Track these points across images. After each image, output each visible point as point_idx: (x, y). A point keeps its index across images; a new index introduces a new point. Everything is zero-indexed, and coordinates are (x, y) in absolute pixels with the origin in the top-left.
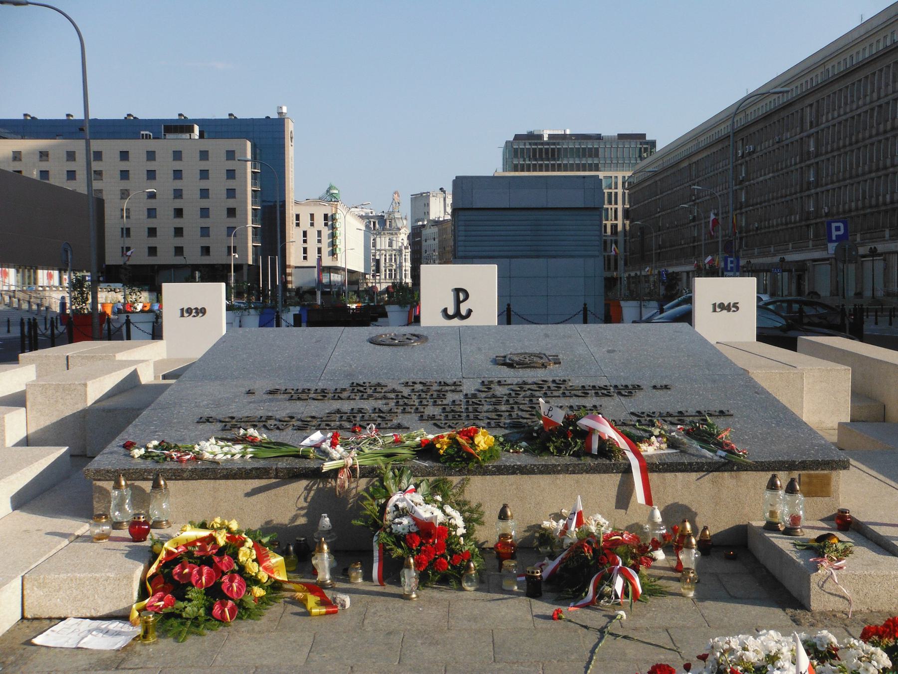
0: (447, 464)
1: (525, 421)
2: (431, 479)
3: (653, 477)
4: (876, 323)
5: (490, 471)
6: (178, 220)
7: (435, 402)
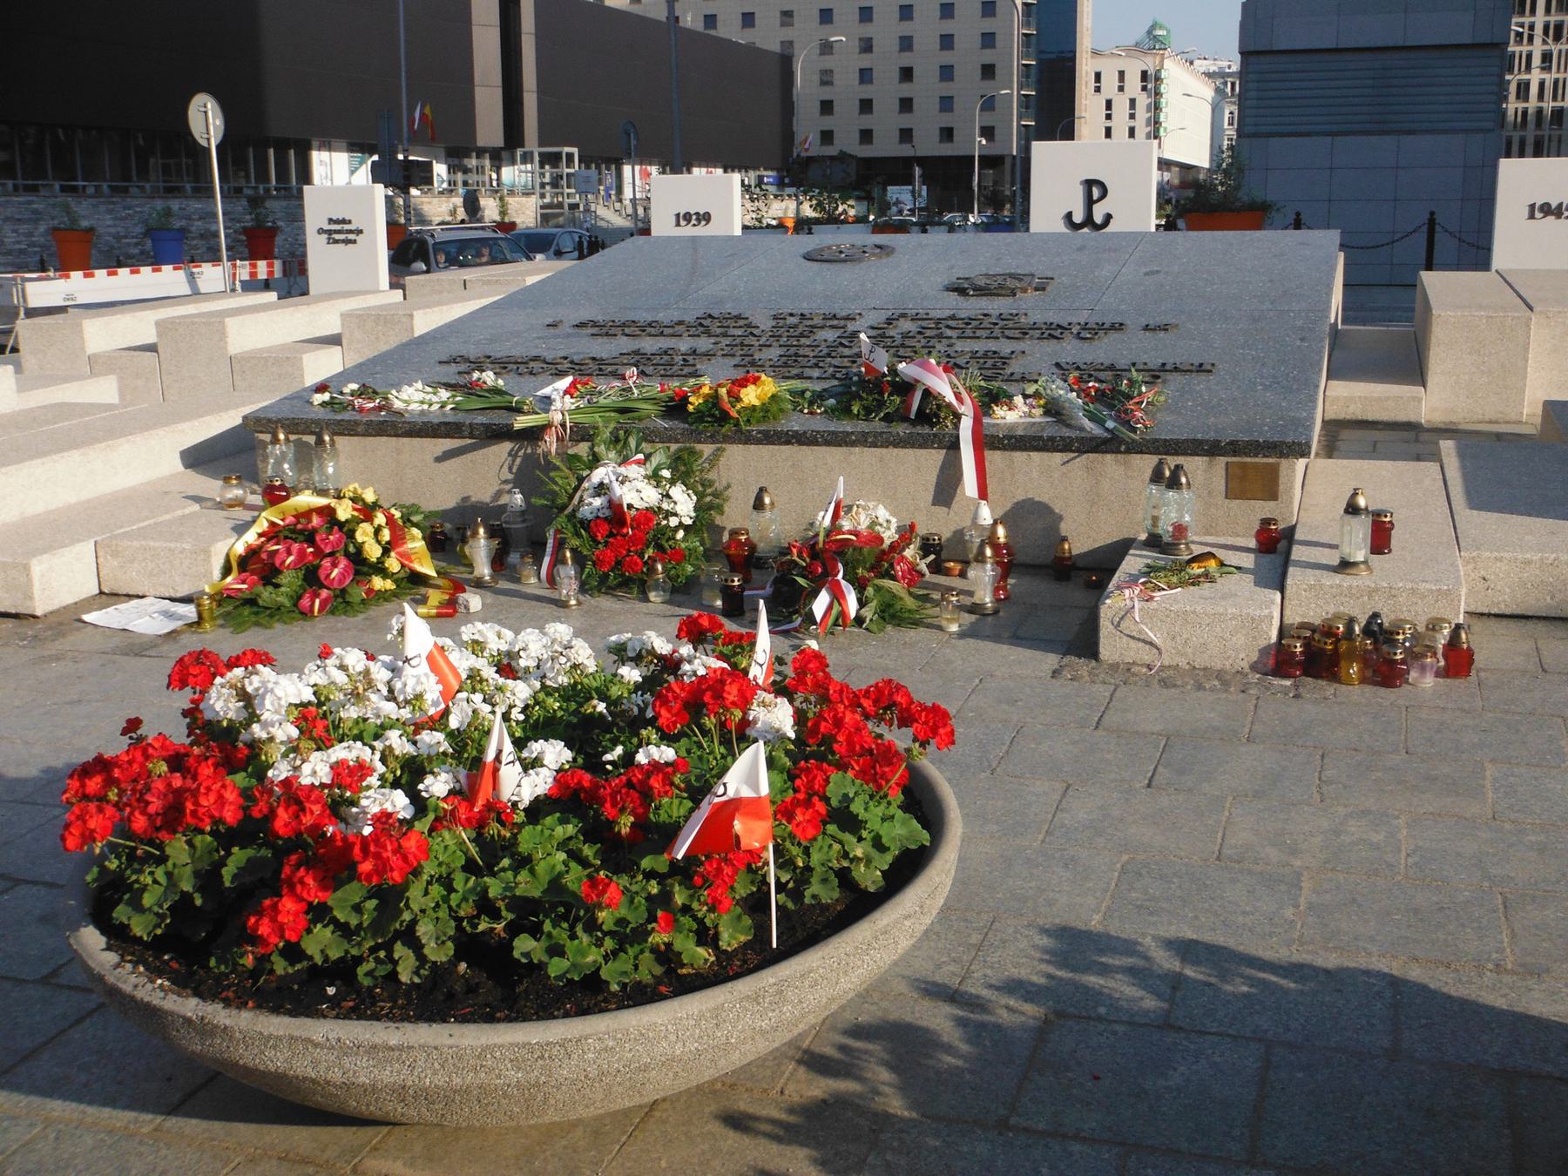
2: (674, 447)
3: (994, 458)
6: (905, 86)
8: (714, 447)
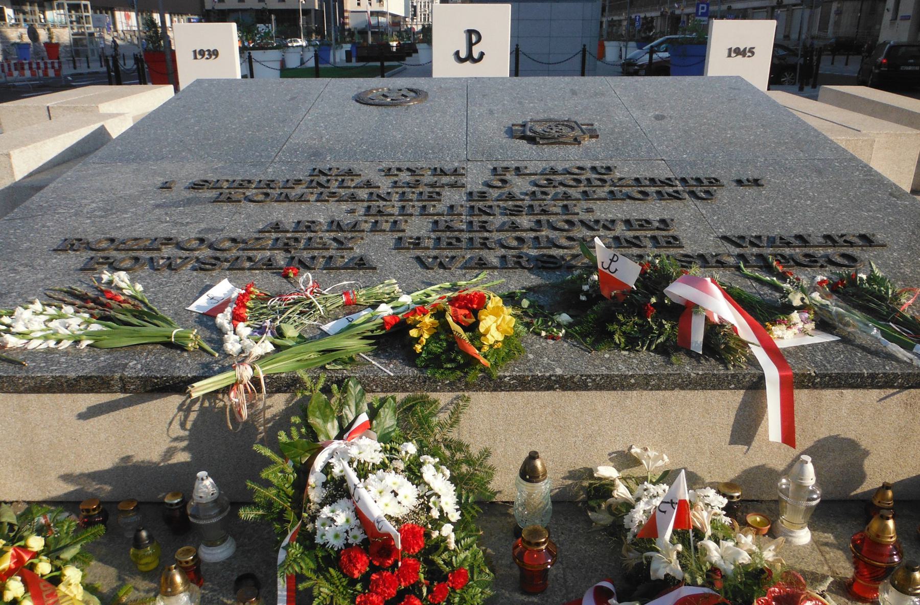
0: (428, 373)
1: (561, 252)
2: (400, 396)
3: (802, 397)
4: (846, 64)
5: (506, 384)
7: (424, 207)
8: (453, 395)
